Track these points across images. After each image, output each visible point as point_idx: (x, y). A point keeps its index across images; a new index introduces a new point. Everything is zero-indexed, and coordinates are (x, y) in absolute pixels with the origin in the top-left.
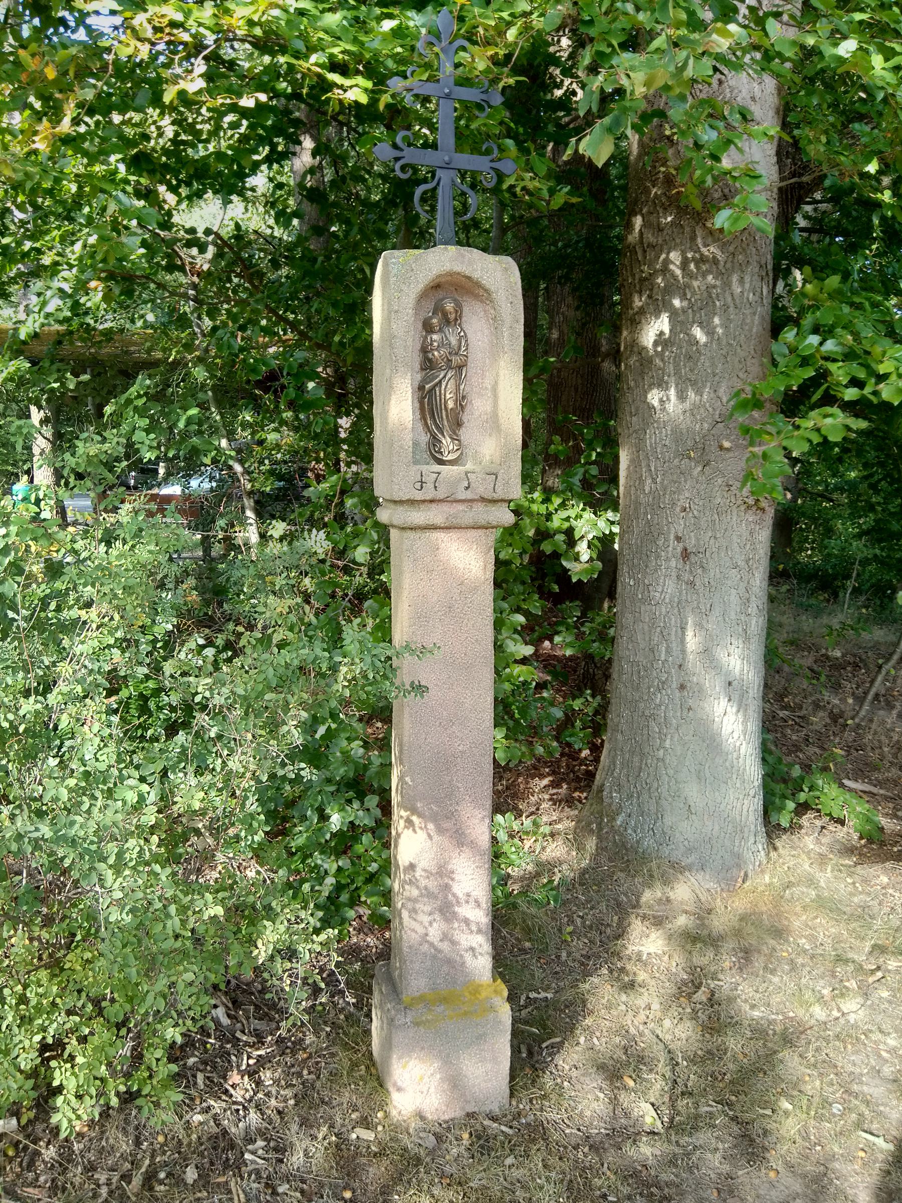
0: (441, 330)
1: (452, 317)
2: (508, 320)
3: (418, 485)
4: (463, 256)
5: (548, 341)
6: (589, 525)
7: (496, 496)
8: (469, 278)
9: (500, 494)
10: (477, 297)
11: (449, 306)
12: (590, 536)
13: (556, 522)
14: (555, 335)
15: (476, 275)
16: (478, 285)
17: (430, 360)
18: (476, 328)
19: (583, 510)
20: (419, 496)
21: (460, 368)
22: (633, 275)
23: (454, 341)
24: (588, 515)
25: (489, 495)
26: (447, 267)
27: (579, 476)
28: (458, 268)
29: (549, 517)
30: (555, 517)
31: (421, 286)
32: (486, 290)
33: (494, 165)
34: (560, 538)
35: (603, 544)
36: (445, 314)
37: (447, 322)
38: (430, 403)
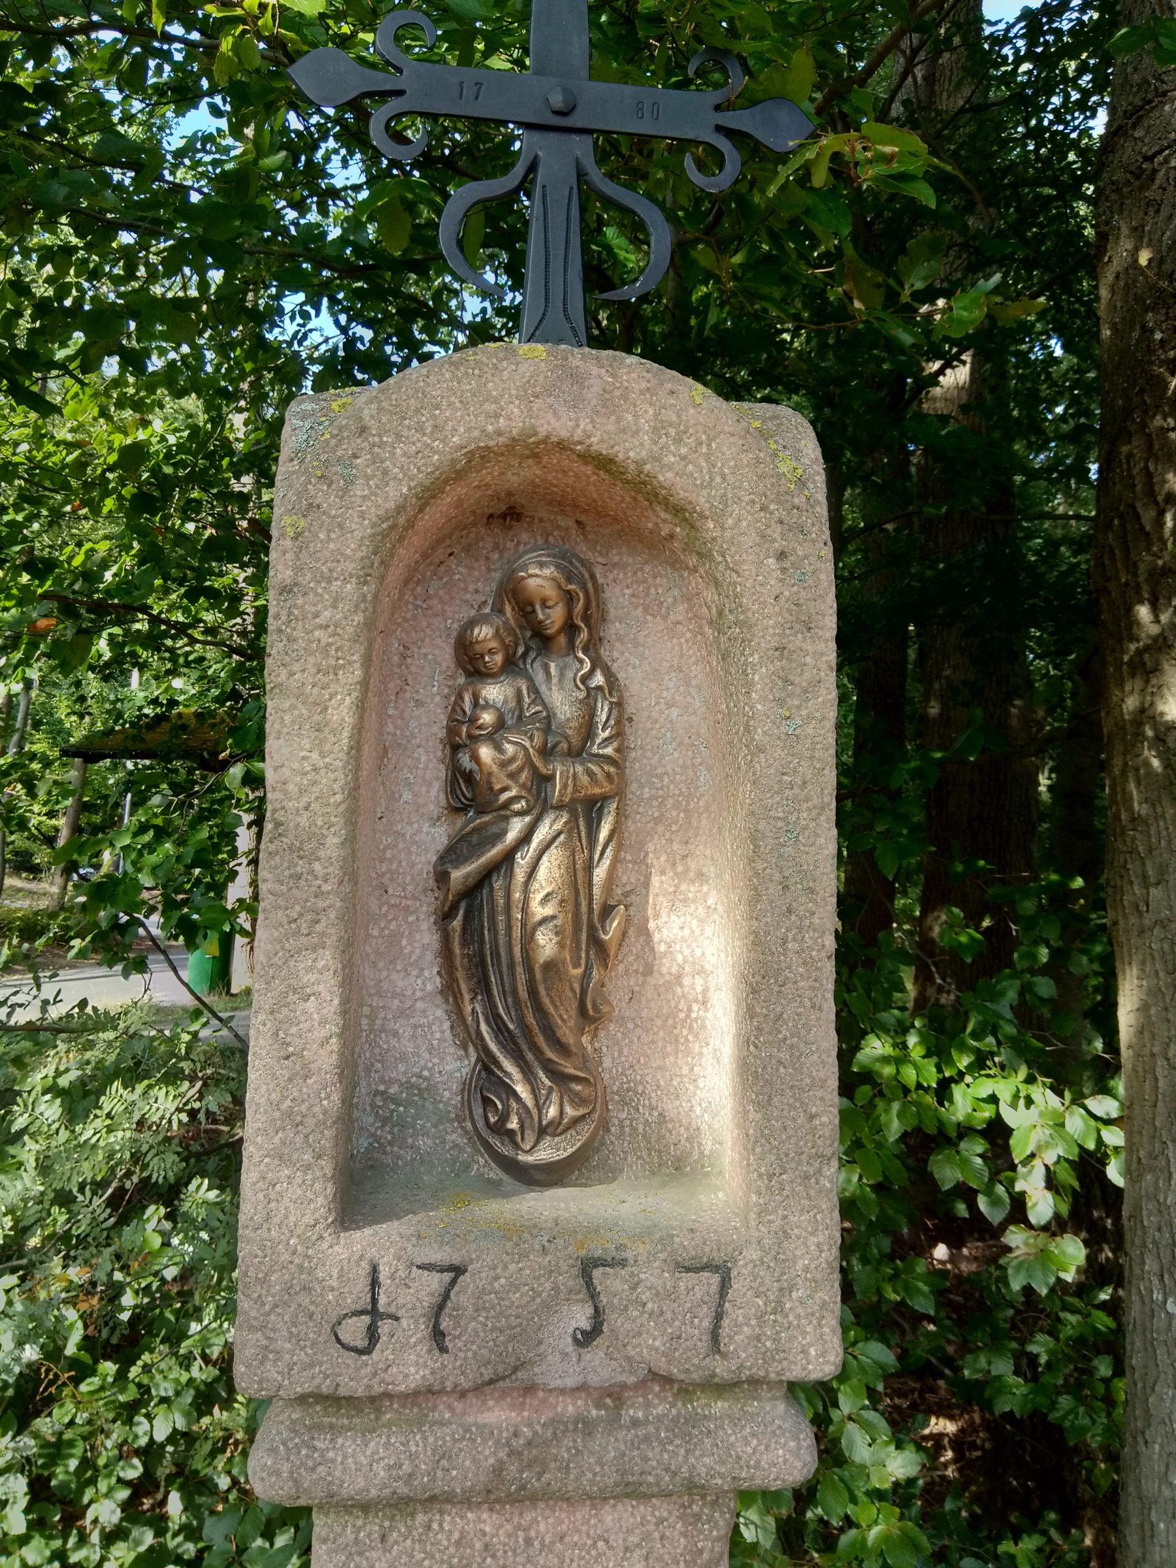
0: (511, 665)
1: (553, 618)
2: (767, 624)
3: (354, 1330)
4: (578, 379)
5: (924, 718)
6: (1044, 1125)
7: (722, 1369)
8: (605, 463)
9: (741, 1353)
10: (654, 546)
11: (540, 578)
12: (1050, 1157)
13: (964, 1103)
14: (934, 710)
15: (632, 450)
16: (645, 490)
17: (469, 777)
18: (658, 661)
19: (1030, 1080)
20: (354, 1377)
21: (589, 810)
22: (1132, 568)
23: (563, 703)
24: (1045, 1097)
25: (693, 1361)
26: (513, 419)
27: (1012, 995)
28: (557, 422)
29: (943, 1090)
30: (957, 1091)
31: (397, 492)
32: (679, 511)
33: (731, 119)
34: (974, 1149)
35: (1089, 1197)
36: (525, 607)
37: (542, 641)
38: (471, 933)
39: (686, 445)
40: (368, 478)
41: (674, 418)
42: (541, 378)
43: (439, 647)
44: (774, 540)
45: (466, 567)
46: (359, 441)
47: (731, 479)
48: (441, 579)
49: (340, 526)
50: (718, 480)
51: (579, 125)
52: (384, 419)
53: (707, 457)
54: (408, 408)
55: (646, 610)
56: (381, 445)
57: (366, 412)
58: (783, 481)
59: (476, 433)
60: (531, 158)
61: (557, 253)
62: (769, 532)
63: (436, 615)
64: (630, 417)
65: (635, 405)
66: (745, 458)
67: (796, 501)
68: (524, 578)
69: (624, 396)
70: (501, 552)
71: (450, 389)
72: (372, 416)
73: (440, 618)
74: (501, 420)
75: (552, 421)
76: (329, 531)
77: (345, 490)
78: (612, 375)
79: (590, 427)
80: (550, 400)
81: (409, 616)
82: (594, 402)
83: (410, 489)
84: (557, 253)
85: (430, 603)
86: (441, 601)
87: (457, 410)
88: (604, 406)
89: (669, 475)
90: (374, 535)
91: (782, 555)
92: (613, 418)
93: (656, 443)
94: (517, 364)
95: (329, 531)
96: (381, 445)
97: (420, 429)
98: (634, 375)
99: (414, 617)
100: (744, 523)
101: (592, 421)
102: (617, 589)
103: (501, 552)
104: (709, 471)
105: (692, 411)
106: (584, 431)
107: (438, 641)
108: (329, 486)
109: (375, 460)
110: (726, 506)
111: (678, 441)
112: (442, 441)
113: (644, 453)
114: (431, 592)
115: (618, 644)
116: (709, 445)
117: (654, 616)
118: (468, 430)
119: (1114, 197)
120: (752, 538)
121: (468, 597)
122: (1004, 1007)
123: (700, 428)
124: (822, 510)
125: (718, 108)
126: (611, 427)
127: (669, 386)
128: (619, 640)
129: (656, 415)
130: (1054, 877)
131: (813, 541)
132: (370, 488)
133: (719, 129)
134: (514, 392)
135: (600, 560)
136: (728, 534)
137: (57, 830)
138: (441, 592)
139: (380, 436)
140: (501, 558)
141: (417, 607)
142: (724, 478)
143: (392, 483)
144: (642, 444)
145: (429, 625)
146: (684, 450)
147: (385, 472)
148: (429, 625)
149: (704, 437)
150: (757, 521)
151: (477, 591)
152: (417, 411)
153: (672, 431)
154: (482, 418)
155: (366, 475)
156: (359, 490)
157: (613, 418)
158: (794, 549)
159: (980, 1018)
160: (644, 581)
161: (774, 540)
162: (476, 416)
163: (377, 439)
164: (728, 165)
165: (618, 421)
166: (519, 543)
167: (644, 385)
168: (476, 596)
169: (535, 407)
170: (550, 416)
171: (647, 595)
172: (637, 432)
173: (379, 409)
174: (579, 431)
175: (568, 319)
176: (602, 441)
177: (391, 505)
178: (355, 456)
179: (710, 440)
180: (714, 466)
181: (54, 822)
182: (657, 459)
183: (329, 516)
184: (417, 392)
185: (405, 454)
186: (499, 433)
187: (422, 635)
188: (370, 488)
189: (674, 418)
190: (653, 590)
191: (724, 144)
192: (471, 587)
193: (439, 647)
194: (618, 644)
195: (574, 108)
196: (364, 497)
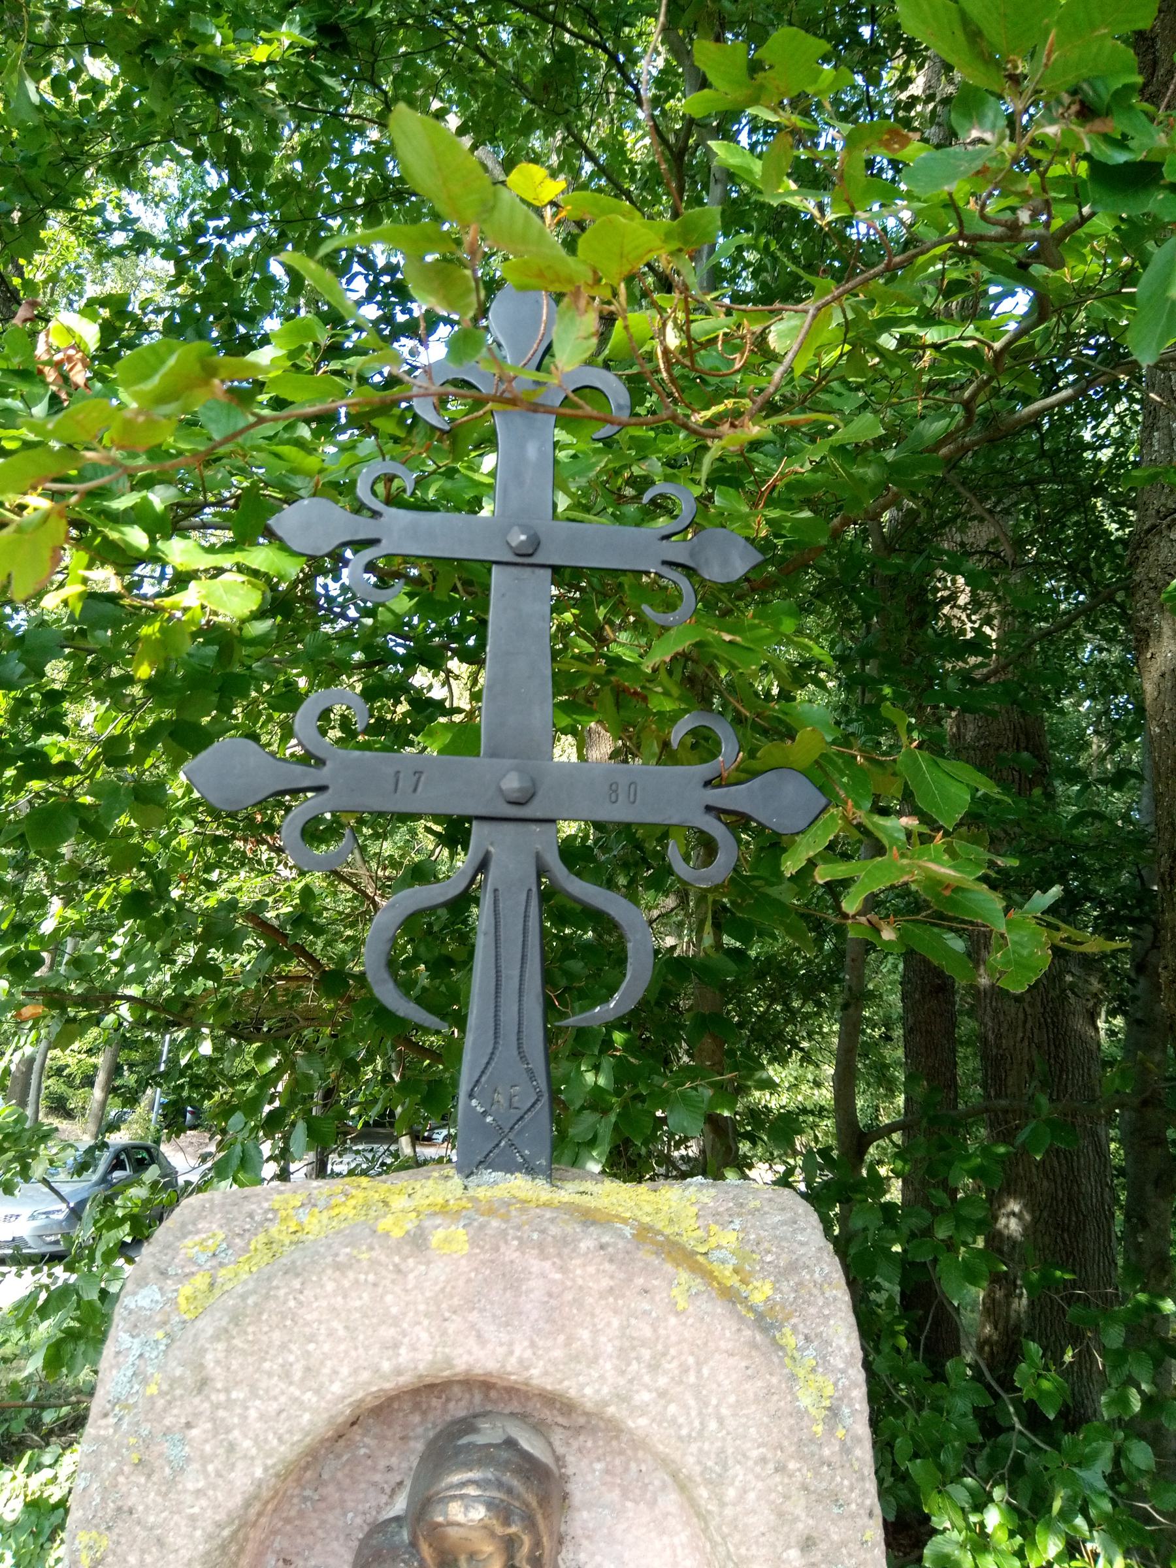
31: (250, 1473)
39: (665, 1372)
40: (205, 1460)
41: (648, 1332)
42: (461, 1283)
43: (334, 1553)
44: (796, 1519)
45: (376, 1437)
46: (197, 1401)
47: (731, 1423)
48: (339, 1456)
49: (160, 1542)
50: (713, 1425)
51: (539, 815)
52: (235, 1365)
53: (697, 1390)
54: (270, 1344)
55: (625, 1493)
56: (229, 1404)
57: (209, 1357)
58: (806, 1422)
59: (365, 1376)
60: (480, 856)
61: (511, 973)
62: (788, 1507)
63: (331, 1508)
64: (585, 1334)
65: (593, 1315)
66: (753, 1388)
67: (826, 1452)
68: (440, 1525)
69: (578, 1302)
70: (424, 1413)
71: (333, 1309)
72: (218, 1362)
73: (338, 1511)
74: (403, 1351)
75: (475, 1349)
76: (143, 1552)
77: (172, 1483)
78: (563, 1269)
79: (528, 1353)
80: (474, 1316)
81: (293, 1513)
82: (535, 1315)
83: (266, 1469)
84: (511, 973)
85: (324, 1491)
86: (340, 1488)
87: (340, 1340)
88: (550, 1320)
89: (643, 1421)
90: (208, 1553)
91: (808, 1544)
92: (561, 1338)
93: (623, 1373)
94: (428, 1263)
95: (143, 1552)
96: (229, 1404)
97: (286, 1374)
98: (591, 1269)
99: (301, 1514)
100: (752, 1496)
101: (533, 1344)
102: (584, 1463)
103: (424, 1413)
104: (700, 1414)
105: (673, 1320)
106: (521, 1361)
107: (335, 1545)
108: (149, 1476)
109: (219, 1428)
110: (725, 1468)
111: (654, 1367)
112: (317, 1392)
113: (605, 1390)
114: (325, 1476)
115: (585, 1543)
116: (699, 1372)
117: (636, 1502)
118: (355, 1372)
119: (1151, 593)
120: (761, 1520)
121: (378, 1477)
122: (1094, 1476)
123: (685, 1346)
124: (864, 1453)
125: (707, 784)
126: (558, 1353)
127: (640, 1281)
128: (588, 1537)
129: (623, 1328)
130: (1142, 1297)
131: (853, 1516)
132: (207, 1475)
133: (709, 809)
134: (422, 1307)
135: (560, 1420)
136: (729, 1511)
137: (95, 1067)
138: (340, 1475)
139: (227, 1391)
140: (422, 1422)
141: (305, 1499)
142: (721, 1421)
143: (240, 1465)
144: (602, 1377)
145: (323, 1522)
146: (662, 1381)
147: (232, 1448)
148: (323, 1522)
149: (691, 1360)
150: (770, 1490)
151: (389, 1469)
152: (284, 1347)
153: (646, 1354)
154: (375, 1350)
155: (202, 1457)
156: (192, 1482)
157: (561, 1338)
158: (826, 1533)
159: (1069, 1492)
160: (622, 1452)
161: (796, 1519)
162: (367, 1348)
163: (222, 1397)
164: (721, 857)
165: (568, 1344)
166: (448, 1400)
167: (605, 1283)
168: (389, 1476)
169: (451, 1328)
170: (471, 1342)
171: (626, 1470)
172: (596, 1359)
173: (229, 1351)
174: (513, 1360)
175: (523, 1057)
176: (546, 1373)
177: (238, 1500)
178: (188, 1425)
179: (699, 1364)
180: (706, 1404)
181: (93, 1060)
182: (623, 1398)
183: (144, 1528)
184: (284, 1318)
185: (262, 1417)
186: (398, 1372)
187: (310, 1539)
188: (207, 1475)
189: (648, 1332)
190: (633, 1465)
191: (716, 829)
192: (382, 1464)
193: (334, 1553)
194: (585, 1543)
195: (533, 795)
196: (199, 1493)
